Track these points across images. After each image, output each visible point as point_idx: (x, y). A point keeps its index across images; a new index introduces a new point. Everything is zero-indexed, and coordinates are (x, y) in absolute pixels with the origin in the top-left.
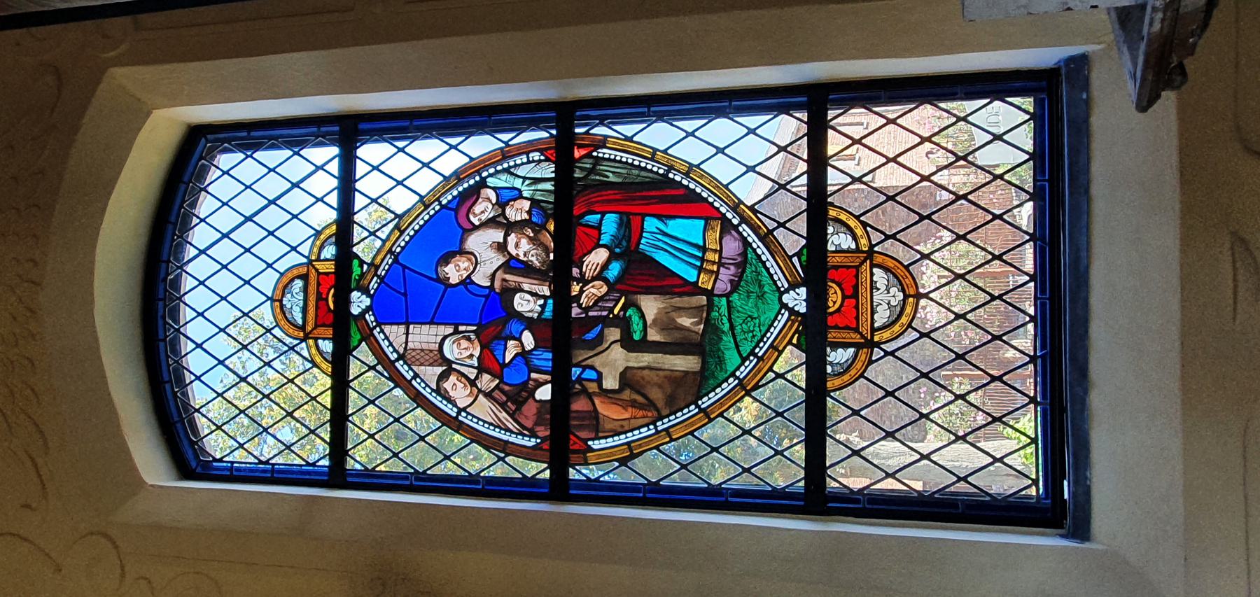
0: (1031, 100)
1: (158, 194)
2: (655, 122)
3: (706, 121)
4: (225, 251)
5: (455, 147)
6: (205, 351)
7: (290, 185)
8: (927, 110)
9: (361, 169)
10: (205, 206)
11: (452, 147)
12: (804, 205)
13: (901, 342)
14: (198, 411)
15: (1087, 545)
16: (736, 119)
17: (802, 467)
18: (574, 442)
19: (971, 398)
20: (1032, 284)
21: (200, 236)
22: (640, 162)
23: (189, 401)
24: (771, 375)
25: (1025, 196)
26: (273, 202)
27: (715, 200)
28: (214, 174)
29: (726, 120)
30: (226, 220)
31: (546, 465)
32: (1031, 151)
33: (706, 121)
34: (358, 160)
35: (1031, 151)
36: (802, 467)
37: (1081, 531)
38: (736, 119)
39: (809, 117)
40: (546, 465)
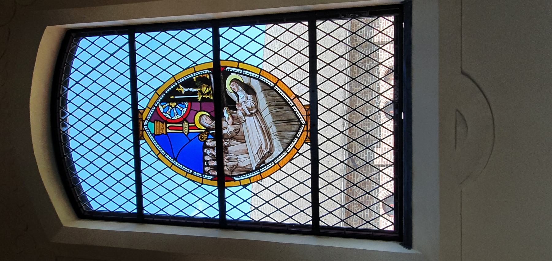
0: (393, 17)
1: (154, 22)
4: (86, 82)
7: (92, 69)
10: (76, 63)
14: (74, 150)
17: (310, 202)
21: (75, 76)
22: (158, 147)
23: (69, 146)
24: (298, 154)
25: (391, 56)
26: (94, 69)
28: (79, 50)
30: (85, 69)
31: (217, 188)
32: (393, 21)
35: (393, 21)
36: (310, 202)
37: (408, 244)
39: (213, 30)
40: (217, 188)
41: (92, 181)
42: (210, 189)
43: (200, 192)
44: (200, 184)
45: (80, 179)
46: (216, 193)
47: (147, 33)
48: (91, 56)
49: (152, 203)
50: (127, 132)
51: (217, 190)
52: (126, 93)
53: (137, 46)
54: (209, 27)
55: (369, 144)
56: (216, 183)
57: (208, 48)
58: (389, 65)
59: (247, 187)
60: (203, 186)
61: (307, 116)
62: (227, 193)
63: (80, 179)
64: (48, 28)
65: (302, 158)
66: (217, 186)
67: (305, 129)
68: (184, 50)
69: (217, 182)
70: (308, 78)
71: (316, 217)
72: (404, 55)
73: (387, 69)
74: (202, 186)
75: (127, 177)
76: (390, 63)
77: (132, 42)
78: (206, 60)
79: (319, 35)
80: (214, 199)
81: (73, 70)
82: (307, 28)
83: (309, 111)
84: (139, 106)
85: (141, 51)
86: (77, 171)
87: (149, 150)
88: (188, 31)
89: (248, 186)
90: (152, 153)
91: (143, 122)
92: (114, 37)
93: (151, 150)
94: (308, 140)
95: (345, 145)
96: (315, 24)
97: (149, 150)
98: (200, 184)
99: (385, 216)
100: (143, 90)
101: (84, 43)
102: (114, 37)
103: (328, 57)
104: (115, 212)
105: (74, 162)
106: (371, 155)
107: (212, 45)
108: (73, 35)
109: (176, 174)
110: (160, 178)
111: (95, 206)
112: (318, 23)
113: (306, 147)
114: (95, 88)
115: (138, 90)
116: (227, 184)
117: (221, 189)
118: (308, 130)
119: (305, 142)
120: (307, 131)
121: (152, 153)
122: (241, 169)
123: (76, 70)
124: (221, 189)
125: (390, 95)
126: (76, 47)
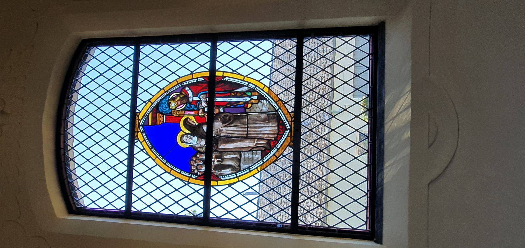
2: (146, 46)
3: (179, 45)
5: (257, 46)
6: (80, 130)
8: (165, 46)
9: (219, 53)
11: (255, 46)
12: (294, 83)
13: (229, 163)
15: (382, 246)
16: (189, 44)
18: (214, 176)
19: (323, 178)
20: (368, 125)
24: (282, 156)
27: (188, 82)
29: (186, 45)
30: (93, 74)
31: (203, 187)
33: (179, 45)
34: (217, 50)
37: (379, 241)
38: (189, 44)
39: (211, 44)
40: (203, 187)
41: (87, 178)
42: (197, 188)
43: (187, 190)
44: (187, 183)
45: (76, 188)
46: (202, 192)
48: (99, 86)
49: (147, 67)
50: (125, 133)
51: (203, 189)
52: (127, 97)
53: (134, 186)
56: (203, 183)
57: (205, 60)
59: (232, 186)
60: (190, 185)
61: (291, 121)
62: (213, 191)
63: (76, 188)
66: (203, 185)
67: (290, 135)
68: (183, 60)
69: (204, 182)
70: (295, 73)
71: (295, 216)
72: (377, 155)
74: (189, 185)
75: (124, 116)
77: (129, 203)
78: (202, 69)
79: (305, 51)
80: (198, 198)
82: (296, 44)
83: (294, 118)
84: (132, 208)
85: (144, 62)
86: (73, 180)
87: (142, 148)
89: (233, 185)
90: (144, 151)
91: (140, 121)
94: (291, 144)
95: (323, 204)
97: (142, 148)
98: (187, 183)
100: (143, 97)
101: (96, 51)
103: (312, 70)
105: (71, 171)
108: (88, 44)
109: (164, 172)
110: (149, 175)
111: (86, 202)
113: (289, 150)
114: (97, 149)
115: (138, 96)
116: (213, 183)
117: (207, 187)
118: (292, 135)
119: (288, 145)
120: (291, 136)
121: (144, 151)
123: (83, 97)
124: (207, 187)
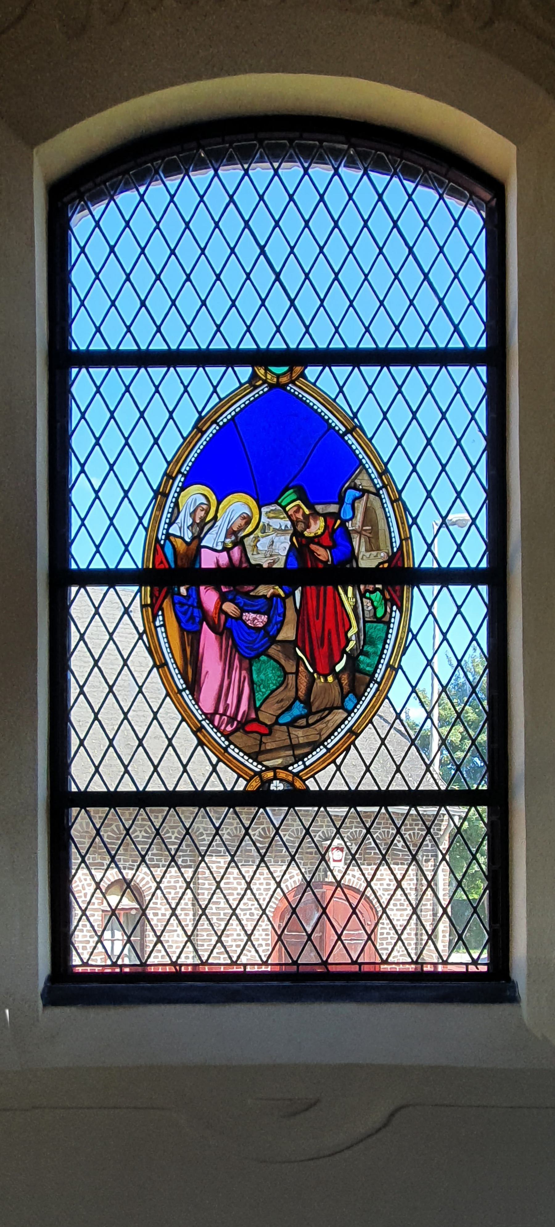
39: (483, 569)
47: (484, 231)
54: (489, 562)
55: (109, 837)
58: (78, 886)
64: (513, 148)
65: (116, 670)
73: (121, 877)
76: (80, 888)
81: (410, 186)
88: (484, 402)
92: (482, 259)
93: (222, 396)
96: (482, 583)
99: (279, 894)
102: (482, 259)
104: (70, 285)
106: (191, 861)
107: (452, 566)
112: (483, 589)
122: (176, 589)
125: (83, 892)
126: (465, 196)
